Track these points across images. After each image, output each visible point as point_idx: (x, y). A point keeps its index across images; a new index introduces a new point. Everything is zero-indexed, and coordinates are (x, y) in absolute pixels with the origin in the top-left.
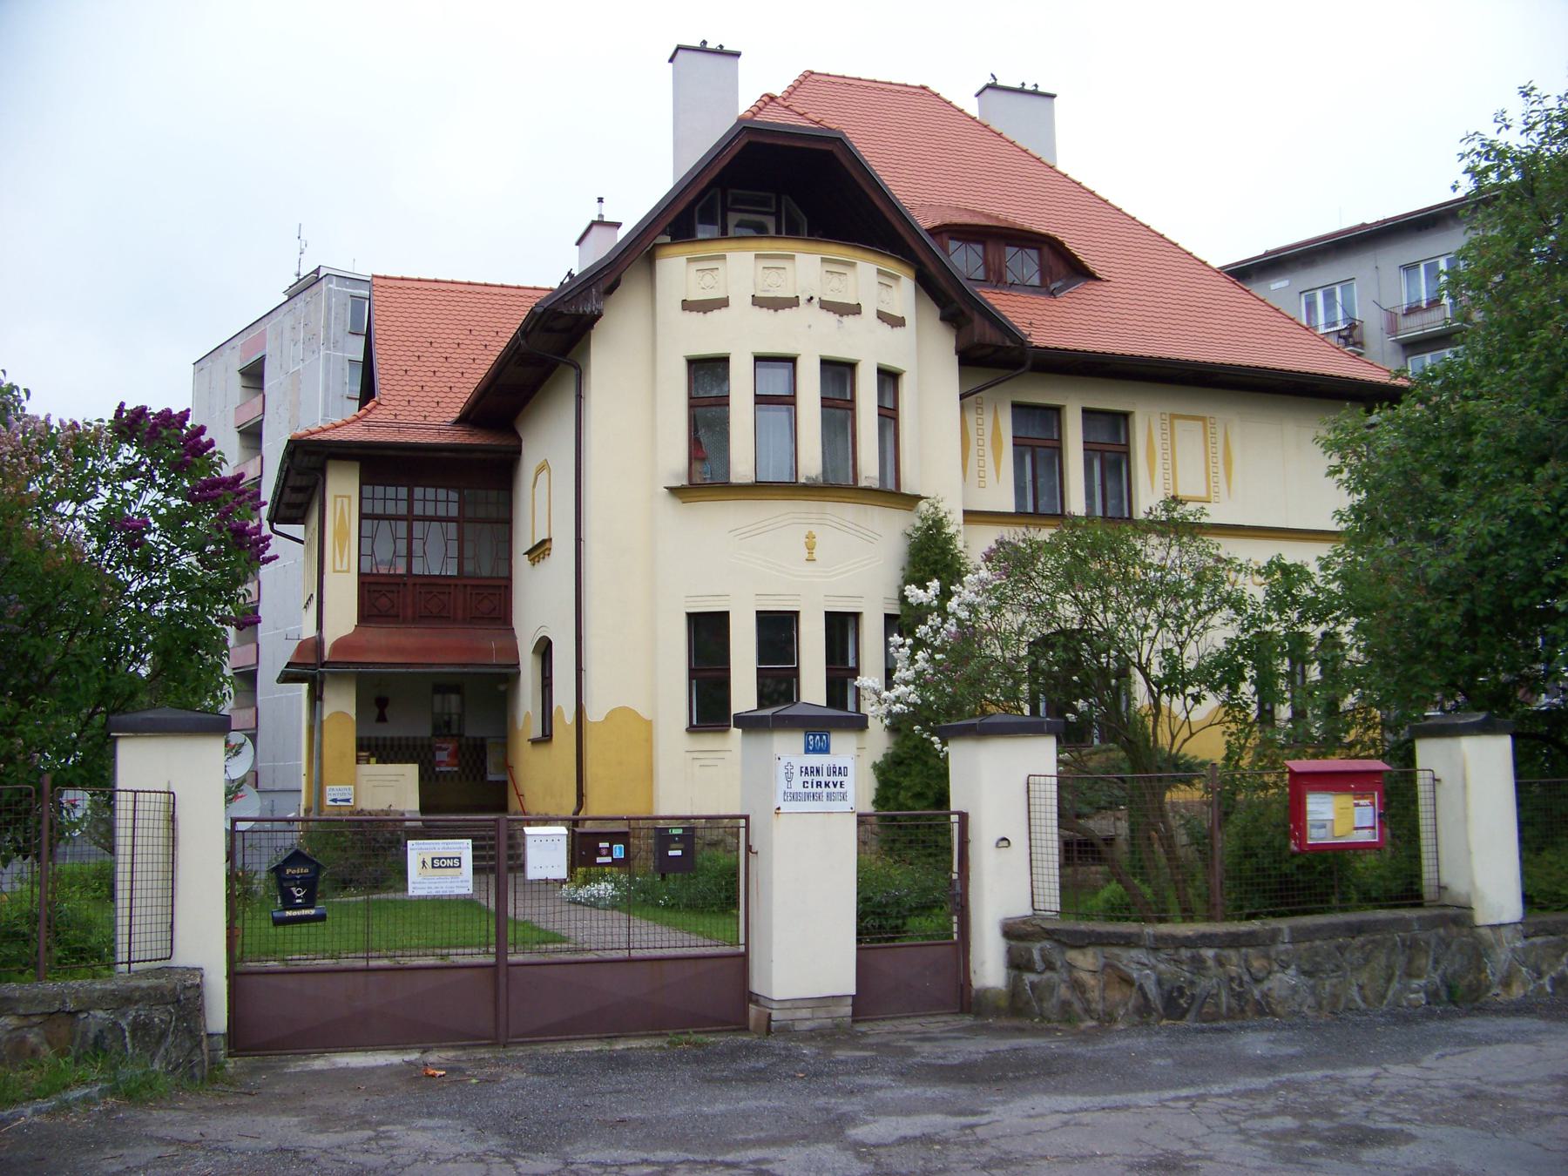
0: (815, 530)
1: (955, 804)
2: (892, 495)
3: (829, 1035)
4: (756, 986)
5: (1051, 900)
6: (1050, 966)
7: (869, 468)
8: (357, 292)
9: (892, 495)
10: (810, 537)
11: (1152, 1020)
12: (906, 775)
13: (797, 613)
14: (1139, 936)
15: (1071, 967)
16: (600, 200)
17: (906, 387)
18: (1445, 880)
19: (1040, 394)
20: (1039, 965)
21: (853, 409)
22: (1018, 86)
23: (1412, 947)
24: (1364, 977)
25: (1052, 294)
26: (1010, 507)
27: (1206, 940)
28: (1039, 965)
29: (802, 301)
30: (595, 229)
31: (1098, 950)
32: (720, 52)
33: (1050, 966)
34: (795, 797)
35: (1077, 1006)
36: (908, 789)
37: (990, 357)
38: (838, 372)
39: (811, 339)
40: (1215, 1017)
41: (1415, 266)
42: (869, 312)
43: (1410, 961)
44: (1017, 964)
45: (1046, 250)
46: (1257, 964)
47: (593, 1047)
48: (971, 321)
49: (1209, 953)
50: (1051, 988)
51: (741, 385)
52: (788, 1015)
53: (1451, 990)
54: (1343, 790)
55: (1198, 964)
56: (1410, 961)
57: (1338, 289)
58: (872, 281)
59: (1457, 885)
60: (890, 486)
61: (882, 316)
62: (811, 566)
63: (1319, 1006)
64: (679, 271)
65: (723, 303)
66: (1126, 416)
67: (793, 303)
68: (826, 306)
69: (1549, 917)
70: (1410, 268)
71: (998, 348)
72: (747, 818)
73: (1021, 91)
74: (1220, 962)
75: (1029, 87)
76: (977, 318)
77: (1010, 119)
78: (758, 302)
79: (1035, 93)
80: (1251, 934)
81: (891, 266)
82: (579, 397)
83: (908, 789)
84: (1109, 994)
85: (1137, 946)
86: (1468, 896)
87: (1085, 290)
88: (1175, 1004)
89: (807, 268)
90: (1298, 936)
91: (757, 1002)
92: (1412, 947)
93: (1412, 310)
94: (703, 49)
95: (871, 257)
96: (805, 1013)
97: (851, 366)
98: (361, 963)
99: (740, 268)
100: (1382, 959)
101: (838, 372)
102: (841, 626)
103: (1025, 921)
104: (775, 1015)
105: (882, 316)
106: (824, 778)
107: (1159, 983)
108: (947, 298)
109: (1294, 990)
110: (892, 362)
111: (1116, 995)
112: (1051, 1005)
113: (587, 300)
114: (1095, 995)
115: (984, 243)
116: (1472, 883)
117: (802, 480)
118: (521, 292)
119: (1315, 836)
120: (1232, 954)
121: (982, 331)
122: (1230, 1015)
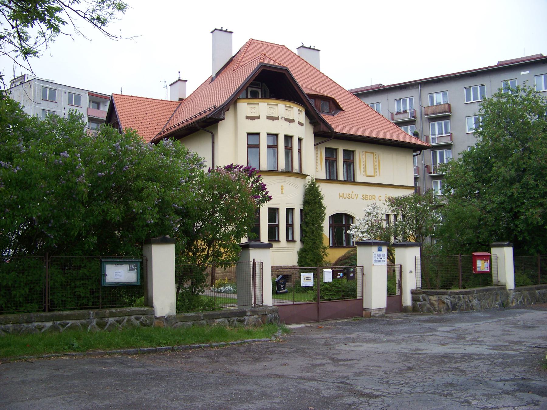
0: (282, 184)
1: (359, 263)
2: (301, 175)
3: (383, 316)
4: (365, 306)
5: (419, 286)
6: (424, 300)
7: (296, 168)
8: (44, 85)
9: (301, 175)
10: (282, 186)
11: (450, 311)
12: (308, 255)
13: (278, 209)
14: (447, 292)
15: (430, 300)
16: (179, 72)
17: (303, 142)
18: (499, 280)
19: (332, 145)
20: (422, 300)
21: (292, 150)
22: (309, 47)
23: (496, 294)
24: (488, 301)
25: (333, 115)
26: (324, 177)
27: (461, 293)
28: (422, 300)
29: (280, 118)
30: (179, 82)
31: (437, 296)
32: (226, 31)
33: (424, 300)
34: (376, 261)
35: (432, 309)
36: (308, 259)
37: (323, 134)
38: (288, 138)
39: (282, 129)
40: (462, 310)
41: (399, 100)
42: (296, 122)
43: (496, 298)
44: (414, 300)
45: (331, 102)
46: (471, 298)
47: (345, 320)
48: (320, 124)
49: (461, 296)
50: (425, 305)
51: (264, 141)
52: (375, 312)
53: (503, 304)
54: (483, 259)
55: (459, 298)
56: (496, 298)
57: (375, 105)
58: (296, 113)
59: (502, 280)
60: (290, 170)
61: (299, 123)
62: (282, 195)
63: (481, 307)
64: (245, 107)
65: (258, 117)
66: (353, 152)
67: (278, 118)
68: (286, 120)
69: (520, 288)
70: (398, 100)
71: (325, 132)
72: (363, 267)
73: (310, 48)
74: (464, 298)
75: (312, 47)
76: (321, 124)
77: (306, 55)
78: (269, 118)
79: (314, 49)
80: (470, 291)
81: (289, 104)
82: (213, 143)
83: (308, 259)
84: (439, 306)
85: (446, 294)
86: (505, 283)
87: (340, 113)
88: (454, 307)
89: (281, 108)
90: (478, 292)
91: (365, 310)
92: (496, 294)
93: (398, 113)
94: (221, 30)
95: (296, 105)
96: (377, 312)
97: (277, 135)
98: (292, 303)
99: (264, 107)
100: (491, 297)
101: (288, 138)
102: (290, 211)
103: (416, 290)
104: (372, 313)
105: (299, 123)
106: (381, 257)
107: (451, 303)
108: (314, 118)
109: (477, 304)
110: (301, 136)
111: (441, 306)
112: (425, 309)
113: (220, 115)
114: (436, 306)
115: (315, 99)
116: (506, 280)
117: (280, 170)
118: (137, 99)
119: (478, 270)
120: (465, 296)
121: (323, 128)
122: (466, 310)
